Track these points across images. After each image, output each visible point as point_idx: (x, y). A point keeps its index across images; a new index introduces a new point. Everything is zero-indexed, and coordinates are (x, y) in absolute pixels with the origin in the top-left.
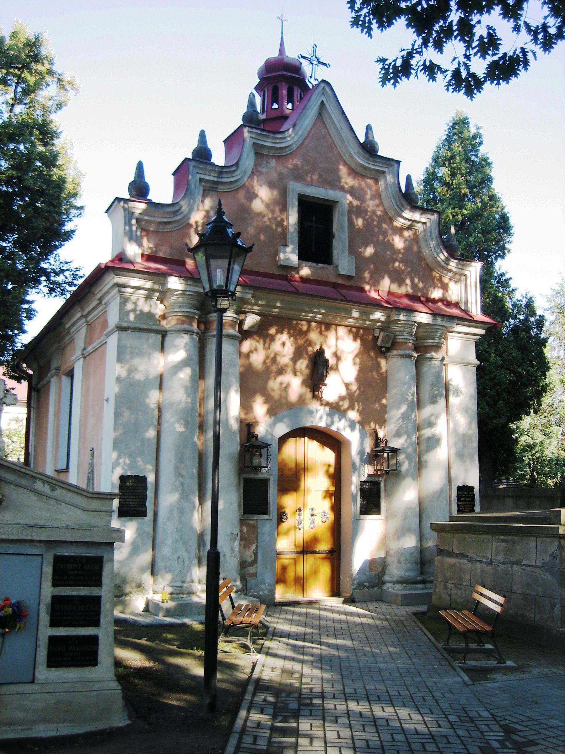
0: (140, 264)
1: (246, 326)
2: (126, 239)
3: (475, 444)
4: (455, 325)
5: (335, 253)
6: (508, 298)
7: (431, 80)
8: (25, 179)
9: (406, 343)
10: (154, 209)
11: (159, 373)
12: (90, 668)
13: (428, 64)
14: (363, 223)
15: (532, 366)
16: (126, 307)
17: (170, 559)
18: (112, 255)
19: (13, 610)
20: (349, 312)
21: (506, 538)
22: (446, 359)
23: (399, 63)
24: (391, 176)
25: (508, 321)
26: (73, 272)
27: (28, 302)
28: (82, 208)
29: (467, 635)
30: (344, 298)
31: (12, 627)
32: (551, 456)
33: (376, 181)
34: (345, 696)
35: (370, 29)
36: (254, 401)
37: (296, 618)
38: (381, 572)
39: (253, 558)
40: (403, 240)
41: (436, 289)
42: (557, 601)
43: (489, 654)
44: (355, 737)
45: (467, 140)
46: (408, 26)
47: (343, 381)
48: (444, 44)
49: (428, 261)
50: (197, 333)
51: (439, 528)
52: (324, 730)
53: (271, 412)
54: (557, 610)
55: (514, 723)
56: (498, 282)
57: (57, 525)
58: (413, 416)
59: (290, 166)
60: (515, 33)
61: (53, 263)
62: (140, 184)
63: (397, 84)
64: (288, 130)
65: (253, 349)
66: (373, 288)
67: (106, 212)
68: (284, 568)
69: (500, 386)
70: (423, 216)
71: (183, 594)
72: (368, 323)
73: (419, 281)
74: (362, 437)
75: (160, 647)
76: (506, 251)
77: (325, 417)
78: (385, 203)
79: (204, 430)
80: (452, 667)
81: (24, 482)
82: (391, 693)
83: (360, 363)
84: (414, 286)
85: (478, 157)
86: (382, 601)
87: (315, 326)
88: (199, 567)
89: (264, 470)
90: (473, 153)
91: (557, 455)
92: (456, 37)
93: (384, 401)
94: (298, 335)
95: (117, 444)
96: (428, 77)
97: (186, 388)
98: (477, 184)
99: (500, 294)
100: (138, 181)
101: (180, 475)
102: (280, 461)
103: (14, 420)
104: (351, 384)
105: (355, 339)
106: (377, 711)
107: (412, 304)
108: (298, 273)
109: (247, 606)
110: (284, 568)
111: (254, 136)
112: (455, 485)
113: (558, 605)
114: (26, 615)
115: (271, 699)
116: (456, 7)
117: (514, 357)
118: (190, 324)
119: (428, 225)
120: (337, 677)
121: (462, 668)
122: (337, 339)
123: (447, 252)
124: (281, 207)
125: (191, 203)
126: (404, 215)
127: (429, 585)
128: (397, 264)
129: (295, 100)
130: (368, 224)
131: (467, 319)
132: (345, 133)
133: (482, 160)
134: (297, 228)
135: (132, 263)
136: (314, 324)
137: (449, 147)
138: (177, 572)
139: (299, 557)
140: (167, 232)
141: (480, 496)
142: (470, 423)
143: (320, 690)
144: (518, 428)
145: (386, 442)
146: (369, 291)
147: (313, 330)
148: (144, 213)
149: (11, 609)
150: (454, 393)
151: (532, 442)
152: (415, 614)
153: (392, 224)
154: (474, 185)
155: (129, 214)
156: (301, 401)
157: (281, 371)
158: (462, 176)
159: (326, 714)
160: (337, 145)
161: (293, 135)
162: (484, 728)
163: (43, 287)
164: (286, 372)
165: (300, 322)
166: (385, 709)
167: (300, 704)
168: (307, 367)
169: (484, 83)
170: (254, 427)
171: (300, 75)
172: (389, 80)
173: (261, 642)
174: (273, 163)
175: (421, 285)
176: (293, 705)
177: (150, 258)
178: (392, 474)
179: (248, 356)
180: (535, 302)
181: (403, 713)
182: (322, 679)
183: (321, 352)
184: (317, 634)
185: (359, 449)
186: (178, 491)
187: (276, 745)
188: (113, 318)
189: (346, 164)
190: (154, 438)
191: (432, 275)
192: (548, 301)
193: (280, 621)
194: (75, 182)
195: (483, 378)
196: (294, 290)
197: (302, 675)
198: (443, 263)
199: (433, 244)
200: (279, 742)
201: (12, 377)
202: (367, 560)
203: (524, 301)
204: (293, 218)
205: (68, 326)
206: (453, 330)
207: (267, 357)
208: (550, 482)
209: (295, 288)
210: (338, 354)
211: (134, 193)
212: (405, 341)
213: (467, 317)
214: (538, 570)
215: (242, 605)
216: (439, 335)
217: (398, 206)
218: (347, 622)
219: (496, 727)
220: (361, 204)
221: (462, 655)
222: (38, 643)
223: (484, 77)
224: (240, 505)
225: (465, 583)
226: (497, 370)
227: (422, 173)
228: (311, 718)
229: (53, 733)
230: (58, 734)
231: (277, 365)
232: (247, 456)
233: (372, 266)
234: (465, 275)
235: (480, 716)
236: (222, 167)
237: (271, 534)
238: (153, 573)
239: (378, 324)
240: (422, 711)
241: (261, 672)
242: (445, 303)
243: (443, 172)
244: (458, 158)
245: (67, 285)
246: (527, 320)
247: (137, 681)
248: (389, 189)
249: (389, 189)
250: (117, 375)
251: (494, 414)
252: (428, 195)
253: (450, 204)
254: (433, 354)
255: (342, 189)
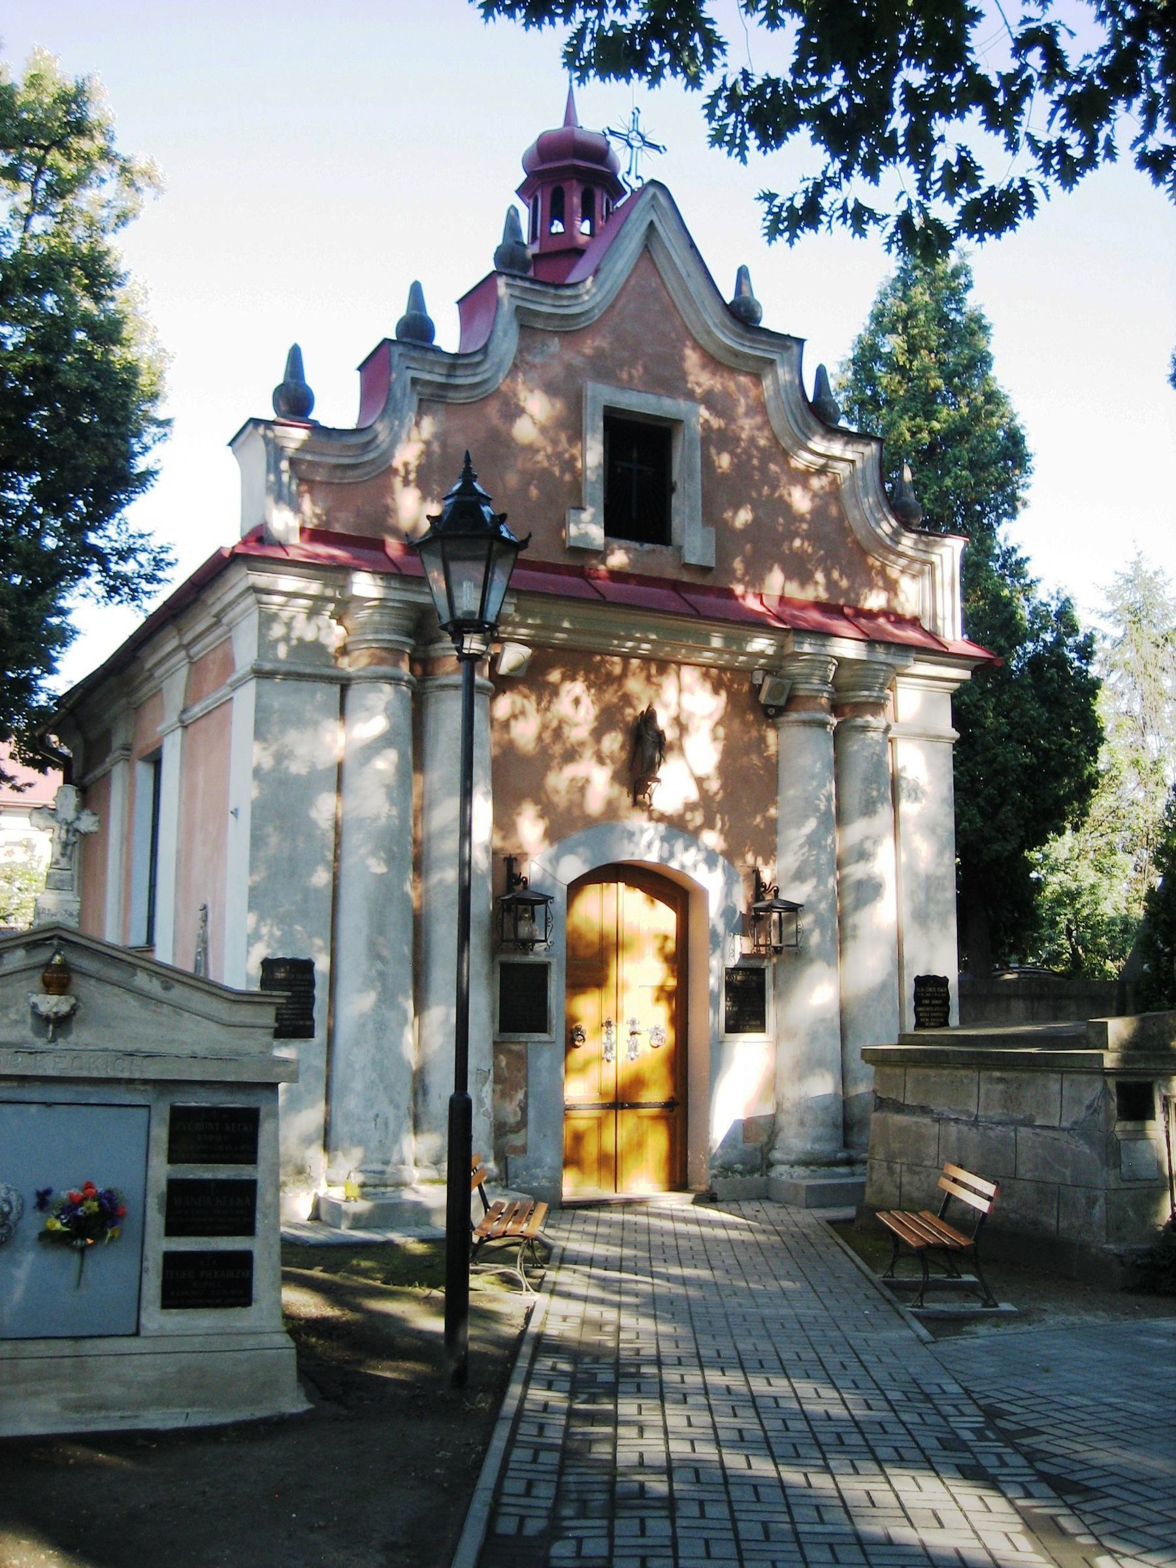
0: (298, 547)
1: (504, 668)
2: (270, 501)
3: (950, 894)
4: (911, 662)
5: (676, 521)
6: (1022, 599)
7: (857, 235)
8: (58, 371)
9: (816, 697)
10: (323, 440)
11: (337, 760)
12: (238, 1309)
13: (851, 206)
14: (732, 463)
15: (1070, 736)
16: (271, 633)
17: (359, 1120)
18: (242, 530)
19: (100, 1205)
20: (703, 641)
21: (1005, 1075)
22: (893, 728)
23: (799, 202)
24: (787, 369)
25: (1021, 645)
26: (154, 554)
27: (62, 612)
28: (166, 423)
29: (928, 1254)
30: (694, 612)
31: (99, 1236)
32: (1112, 914)
33: (757, 378)
34: (700, 1361)
35: (743, 148)
36: (519, 814)
37: (602, 1230)
38: (768, 1143)
39: (519, 1118)
40: (809, 495)
41: (875, 592)
42: (1099, 1193)
43: (968, 1291)
44: (718, 1425)
45: (942, 279)
46: (815, 139)
47: (692, 773)
48: (882, 167)
49: (859, 537)
50: (409, 682)
51: (878, 1059)
52: (664, 1415)
53: (552, 835)
54: (1098, 1211)
55: (1003, 1401)
56: (1003, 566)
57: (175, 1051)
58: (829, 841)
59: (588, 351)
60: (1010, 152)
61: (114, 536)
62: (296, 390)
63: (796, 240)
64: (584, 281)
65: (517, 712)
66: (750, 590)
67: (230, 444)
68: (578, 1138)
69: (1006, 777)
70: (849, 447)
71: (386, 1186)
72: (741, 658)
73: (841, 576)
74: (730, 882)
75: (349, 1283)
76: (1019, 504)
77: (657, 844)
78: (776, 423)
79: (424, 868)
80: (899, 1313)
81: (114, 974)
82: (784, 1356)
83: (726, 739)
84: (831, 585)
85: (962, 314)
86: (768, 1198)
87: (639, 667)
88: (415, 1133)
89: (540, 947)
90: (954, 306)
91: (1124, 912)
92: (902, 157)
93: (772, 812)
94: (604, 683)
95: (257, 899)
96: (852, 229)
97: (387, 786)
98: (961, 369)
99: (1006, 592)
100: (292, 386)
101: (379, 957)
102: (570, 928)
103: (19, 844)
104: (708, 778)
105: (716, 691)
106: (759, 1385)
107: (828, 621)
108: (604, 562)
109: (512, 1205)
110: (578, 1138)
111: (517, 293)
112: (909, 975)
113: (1101, 1201)
114: (122, 1216)
115: (565, 1367)
116: (902, 108)
117: (1032, 718)
118: (396, 665)
119: (859, 465)
120: (683, 1331)
121: (917, 1316)
122: (680, 691)
123: (897, 519)
124: (570, 432)
125: (396, 428)
126: (811, 445)
127: (858, 1169)
128: (797, 543)
129: (598, 216)
130: (740, 465)
131: (935, 651)
132: (696, 284)
133: (971, 320)
134: (601, 471)
135: (281, 546)
136: (635, 662)
137: (904, 293)
138: (373, 1144)
139: (607, 1114)
140: (350, 484)
141: (960, 996)
142: (940, 853)
143: (653, 1352)
144: (1046, 857)
145: (777, 892)
146: (743, 597)
147: (634, 674)
148: (305, 447)
149: (96, 1204)
150: (909, 796)
151: (1073, 886)
152: (832, 1223)
153: (788, 463)
154: (955, 371)
155: (276, 451)
156: (611, 811)
157: (571, 755)
158: (931, 351)
159: (665, 1390)
160: (682, 312)
161: (594, 290)
162: (950, 1410)
163: (93, 582)
164: (580, 757)
165: (608, 658)
166: (772, 1381)
167: (618, 1375)
168: (622, 747)
169: (955, 239)
170: (519, 865)
171: (607, 166)
172: (781, 232)
173: (540, 1272)
174: (555, 345)
175: (844, 583)
176: (606, 1376)
177: (315, 535)
178: (789, 952)
179: (506, 725)
180: (1077, 608)
181: (805, 1388)
182: (657, 1334)
183: (649, 717)
184: (643, 1258)
185: (723, 906)
186: (374, 988)
187: (579, 1437)
188: (245, 653)
189: (697, 346)
190: (326, 885)
191: (865, 561)
192: (1108, 597)
193: (573, 1236)
194: (154, 369)
195: (971, 760)
196: (596, 596)
197: (619, 1328)
198: (888, 541)
199: (869, 501)
200: (583, 1434)
201: (28, 762)
202: (740, 1120)
203: (1054, 606)
204: (593, 455)
205: (149, 665)
206: (907, 671)
207: (544, 727)
208: (1110, 966)
209: (598, 592)
210: (683, 720)
211: (283, 408)
212: (814, 694)
213: (936, 646)
214: (1064, 1136)
215: (502, 1205)
216: (881, 681)
217: (800, 429)
218: (702, 1238)
219: (970, 1409)
220: (727, 425)
221: (917, 1294)
222: (145, 1264)
223: (955, 228)
224: (493, 1016)
225: (928, 1163)
226: (1001, 743)
227: (850, 345)
228: (639, 1395)
229: (181, 1423)
230: (186, 1425)
231: (564, 743)
232: (508, 921)
233: (748, 547)
234: (932, 563)
235: (944, 1392)
236: (456, 356)
237: (553, 1070)
238: (326, 1147)
239: (762, 661)
240: (839, 1383)
241: (544, 1324)
242: (892, 618)
243: (892, 344)
244: (922, 316)
245: (143, 581)
246: (1059, 643)
247: (314, 1340)
248: (782, 393)
249: (782, 393)
250: (254, 763)
251: (994, 833)
252: (862, 392)
253: (905, 410)
254: (869, 718)
255: (690, 395)
